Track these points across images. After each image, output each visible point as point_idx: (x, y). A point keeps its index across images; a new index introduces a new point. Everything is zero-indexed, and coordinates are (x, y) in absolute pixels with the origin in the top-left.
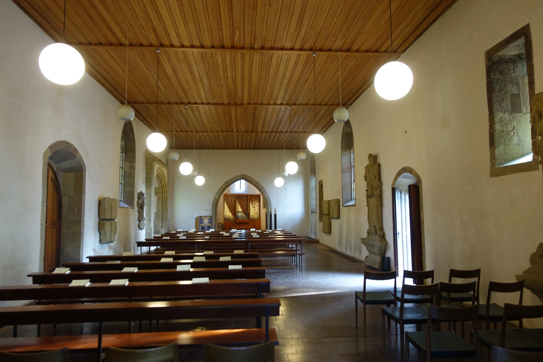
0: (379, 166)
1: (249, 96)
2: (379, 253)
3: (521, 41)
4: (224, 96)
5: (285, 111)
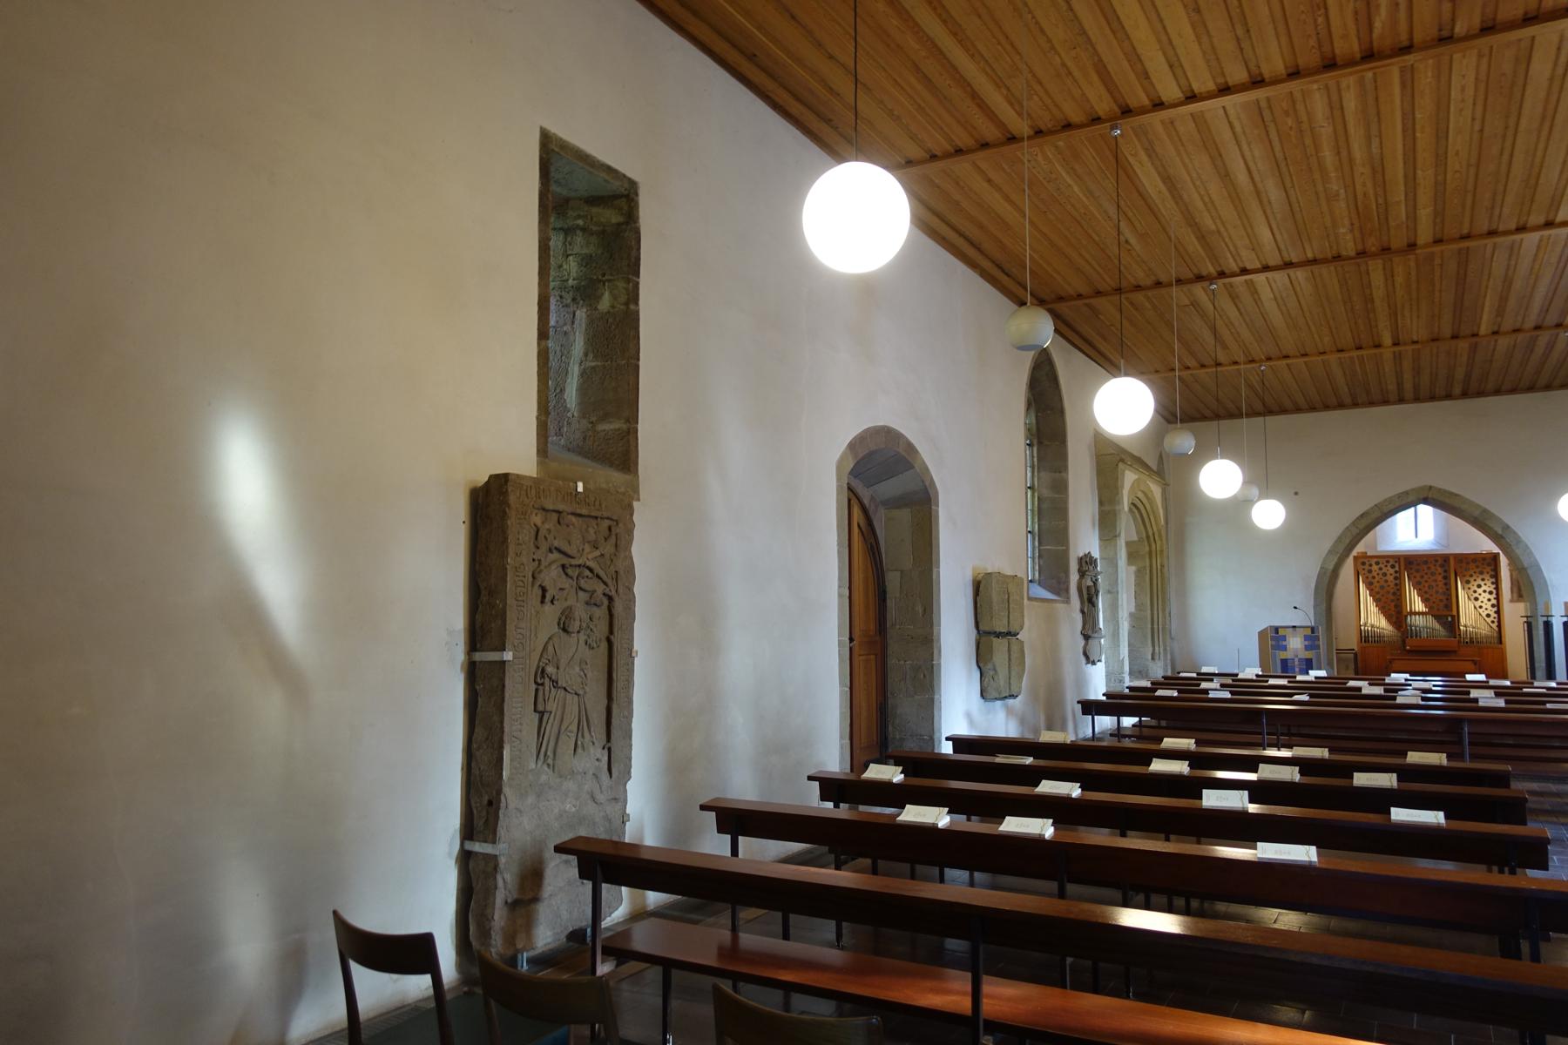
1: (1439, 214)
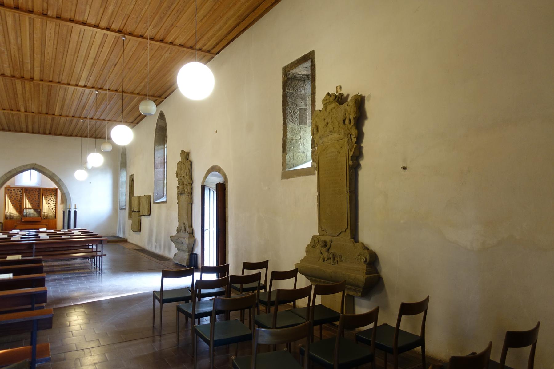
0: (191, 163)
1: (42, 71)
2: (187, 250)
3: (308, 64)
4: (5, 66)
5: (90, 95)
